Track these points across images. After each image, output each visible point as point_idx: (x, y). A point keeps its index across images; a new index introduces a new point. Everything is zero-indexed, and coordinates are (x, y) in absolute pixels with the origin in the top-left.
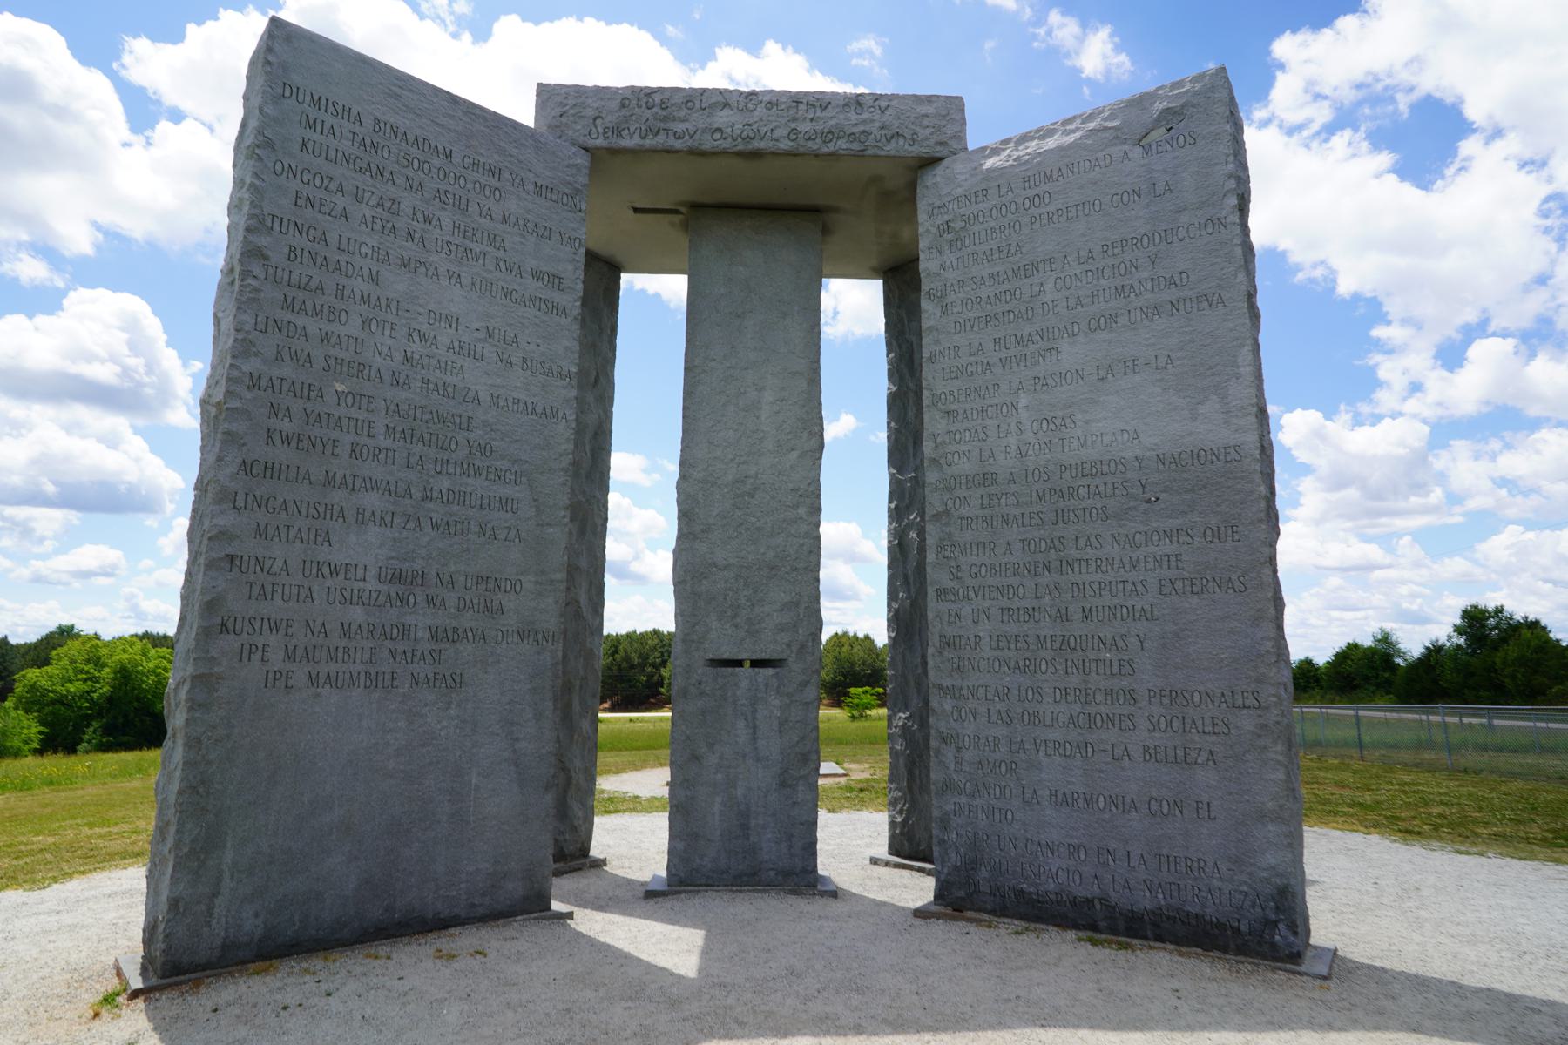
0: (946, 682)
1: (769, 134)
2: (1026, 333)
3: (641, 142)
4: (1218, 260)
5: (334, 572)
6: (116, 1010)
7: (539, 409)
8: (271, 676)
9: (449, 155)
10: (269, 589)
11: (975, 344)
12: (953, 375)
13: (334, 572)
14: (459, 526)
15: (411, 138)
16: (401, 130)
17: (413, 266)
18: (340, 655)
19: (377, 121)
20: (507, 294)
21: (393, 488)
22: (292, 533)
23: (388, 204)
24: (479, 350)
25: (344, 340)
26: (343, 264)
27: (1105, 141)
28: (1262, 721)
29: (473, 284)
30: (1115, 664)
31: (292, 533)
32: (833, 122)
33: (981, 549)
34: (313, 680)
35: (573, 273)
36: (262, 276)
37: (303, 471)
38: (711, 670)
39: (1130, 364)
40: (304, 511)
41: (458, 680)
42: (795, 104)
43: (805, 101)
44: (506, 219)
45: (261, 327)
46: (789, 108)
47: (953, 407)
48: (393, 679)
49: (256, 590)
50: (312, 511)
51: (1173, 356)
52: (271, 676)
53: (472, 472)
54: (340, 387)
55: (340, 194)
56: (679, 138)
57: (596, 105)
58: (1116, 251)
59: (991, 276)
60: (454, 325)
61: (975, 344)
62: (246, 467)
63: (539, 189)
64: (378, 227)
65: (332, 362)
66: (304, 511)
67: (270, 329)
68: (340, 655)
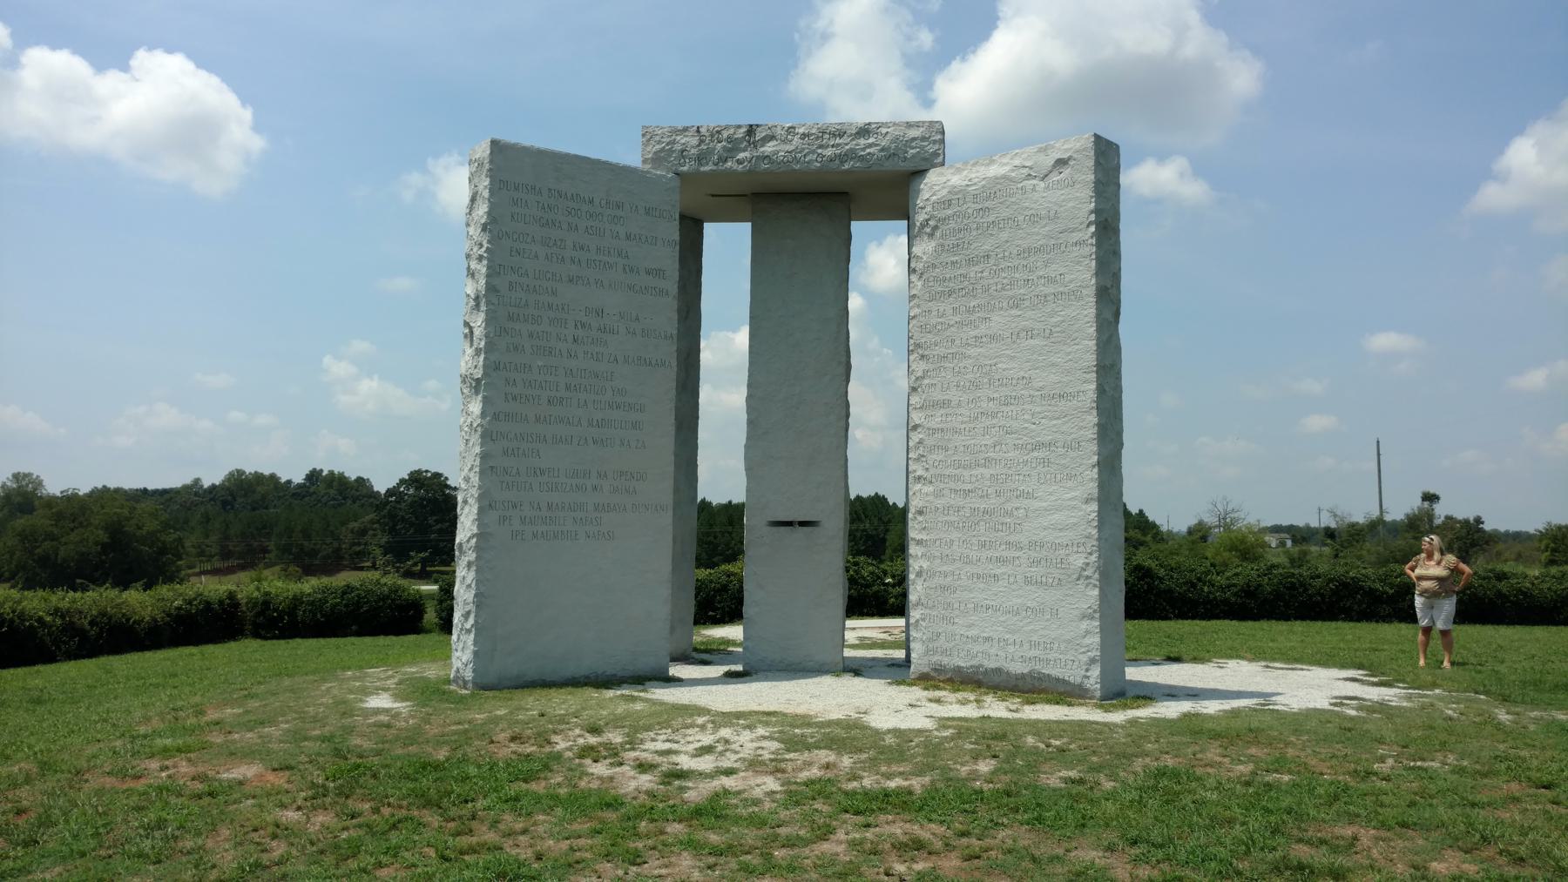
0: (919, 537)
1: (802, 158)
2: (972, 305)
3: (715, 168)
4: (1081, 268)
5: (542, 473)
6: (1110, 220)
7: (653, 362)
8: (514, 533)
9: (591, 201)
10: (510, 484)
11: (941, 310)
12: (928, 330)
13: (542, 473)
14: (609, 441)
15: (569, 195)
16: (563, 193)
17: (575, 280)
18: (548, 521)
19: (550, 190)
20: (631, 288)
21: (571, 421)
22: (521, 452)
23: (559, 243)
24: (616, 327)
25: (540, 334)
26: (537, 287)
27: (1023, 176)
28: (1087, 561)
29: (610, 285)
30: (1012, 525)
31: (521, 452)
32: (847, 147)
33: (940, 451)
34: (535, 536)
35: (672, 231)
36: (497, 302)
37: (524, 416)
38: (769, 528)
39: (1030, 333)
40: (526, 439)
41: (611, 535)
42: (821, 134)
43: (828, 131)
44: (628, 237)
45: (498, 334)
46: (817, 138)
47: (926, 353)
48: (576, 535)
49: (504, 485)
50: (530, 439)
51: (1054, 330)
52: (514, 533)
53: (615, 407)
54: (540, 363)
55: (533, 243)
56: (741, 163)
57: (683, 141)
58: (1026, 255)
59: (953, 263)
60: (600, 314)
61: (941, 310)
62: (496, 417)
63: (648, 212)
64: (555, 259)
65: (535, 349)
66: (526, 439)
67: (502, 334)
68: (548, 521)
